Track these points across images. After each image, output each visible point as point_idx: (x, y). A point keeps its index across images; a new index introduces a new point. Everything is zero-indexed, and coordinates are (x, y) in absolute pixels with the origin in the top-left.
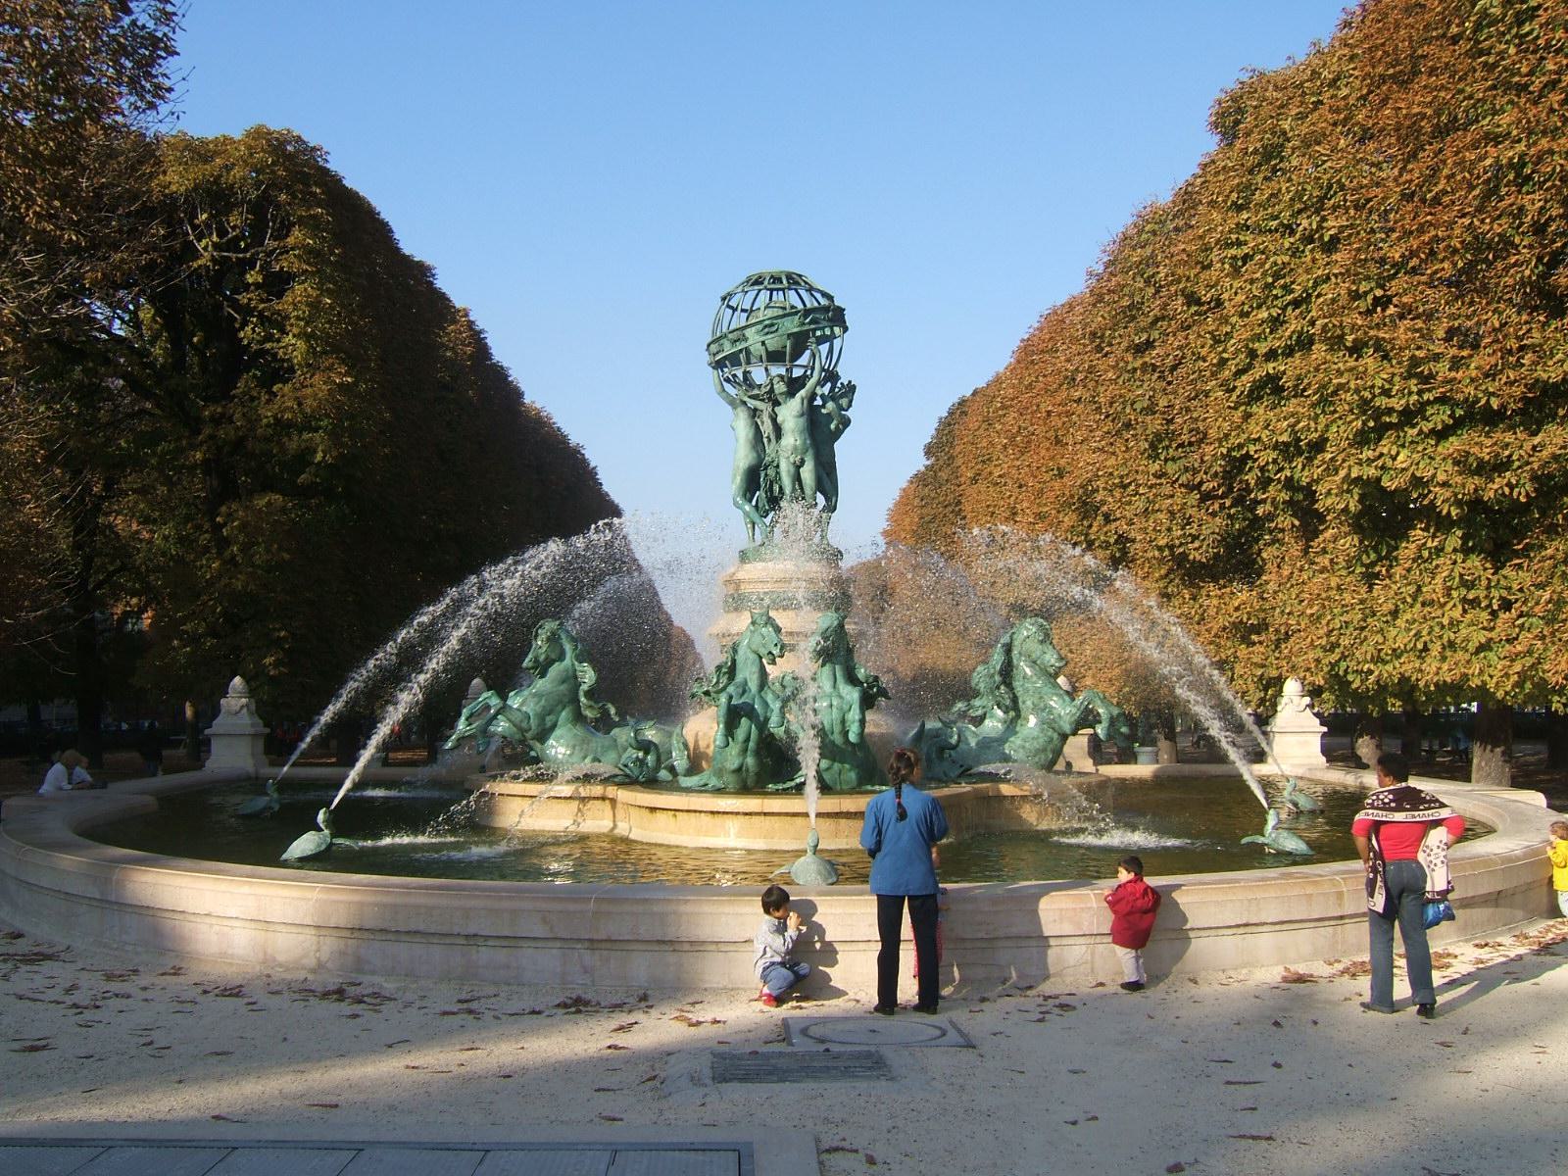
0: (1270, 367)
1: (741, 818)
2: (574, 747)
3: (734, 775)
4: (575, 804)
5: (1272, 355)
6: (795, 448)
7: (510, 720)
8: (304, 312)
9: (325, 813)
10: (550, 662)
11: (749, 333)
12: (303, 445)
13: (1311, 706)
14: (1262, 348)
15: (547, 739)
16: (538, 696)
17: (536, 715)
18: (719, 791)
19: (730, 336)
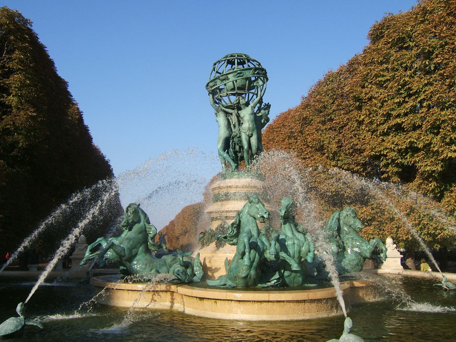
0: (398, 120)
1: (256, 305)
2: (146, 265)
5: (398, 116)
6: (249, 129)
7: (115, 251)
8: (18, 85)
9: (22, 305)
10: (134, 223)
11: (229, 76)
12: (14, 140)
13: (396, 248)
14: (394, 113)
15: (133, 261)
16: (129, 239)
17: (128, 249)
18: (234, 289)
19: (221, 78)
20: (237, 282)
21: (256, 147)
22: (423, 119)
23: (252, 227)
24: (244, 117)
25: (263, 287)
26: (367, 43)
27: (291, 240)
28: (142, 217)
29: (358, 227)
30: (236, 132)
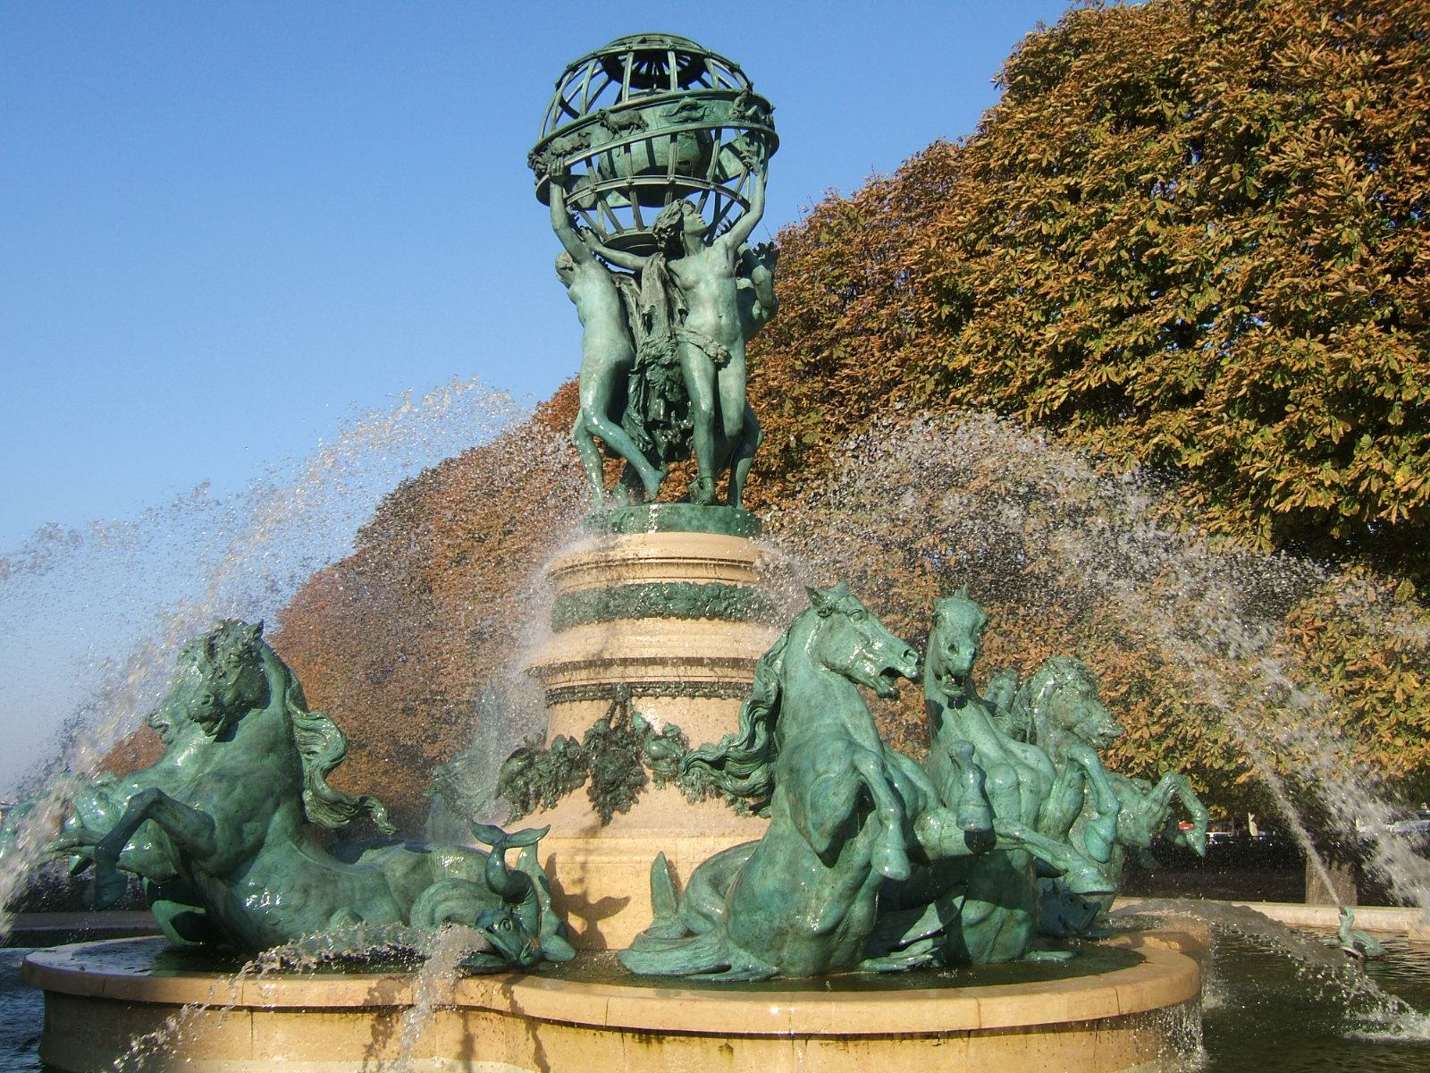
2: (306, 891)
3: (813, 945)
4: (367, 1020)
6: (718, 332)
7: (168, 829)
14: (1098, 347)
17: (226, 819)
18: (767, 984)
19: (613, 118)
20: (785, 954)
21: (739, 409)
22: (1212, 370)
23: (853, 715)
24: (697, 282)
25: (883, 973)
26: (994, 99)
27: (1003, 769)
28: (275, 680)
29: (1101, 731)
30: (660, 346)
